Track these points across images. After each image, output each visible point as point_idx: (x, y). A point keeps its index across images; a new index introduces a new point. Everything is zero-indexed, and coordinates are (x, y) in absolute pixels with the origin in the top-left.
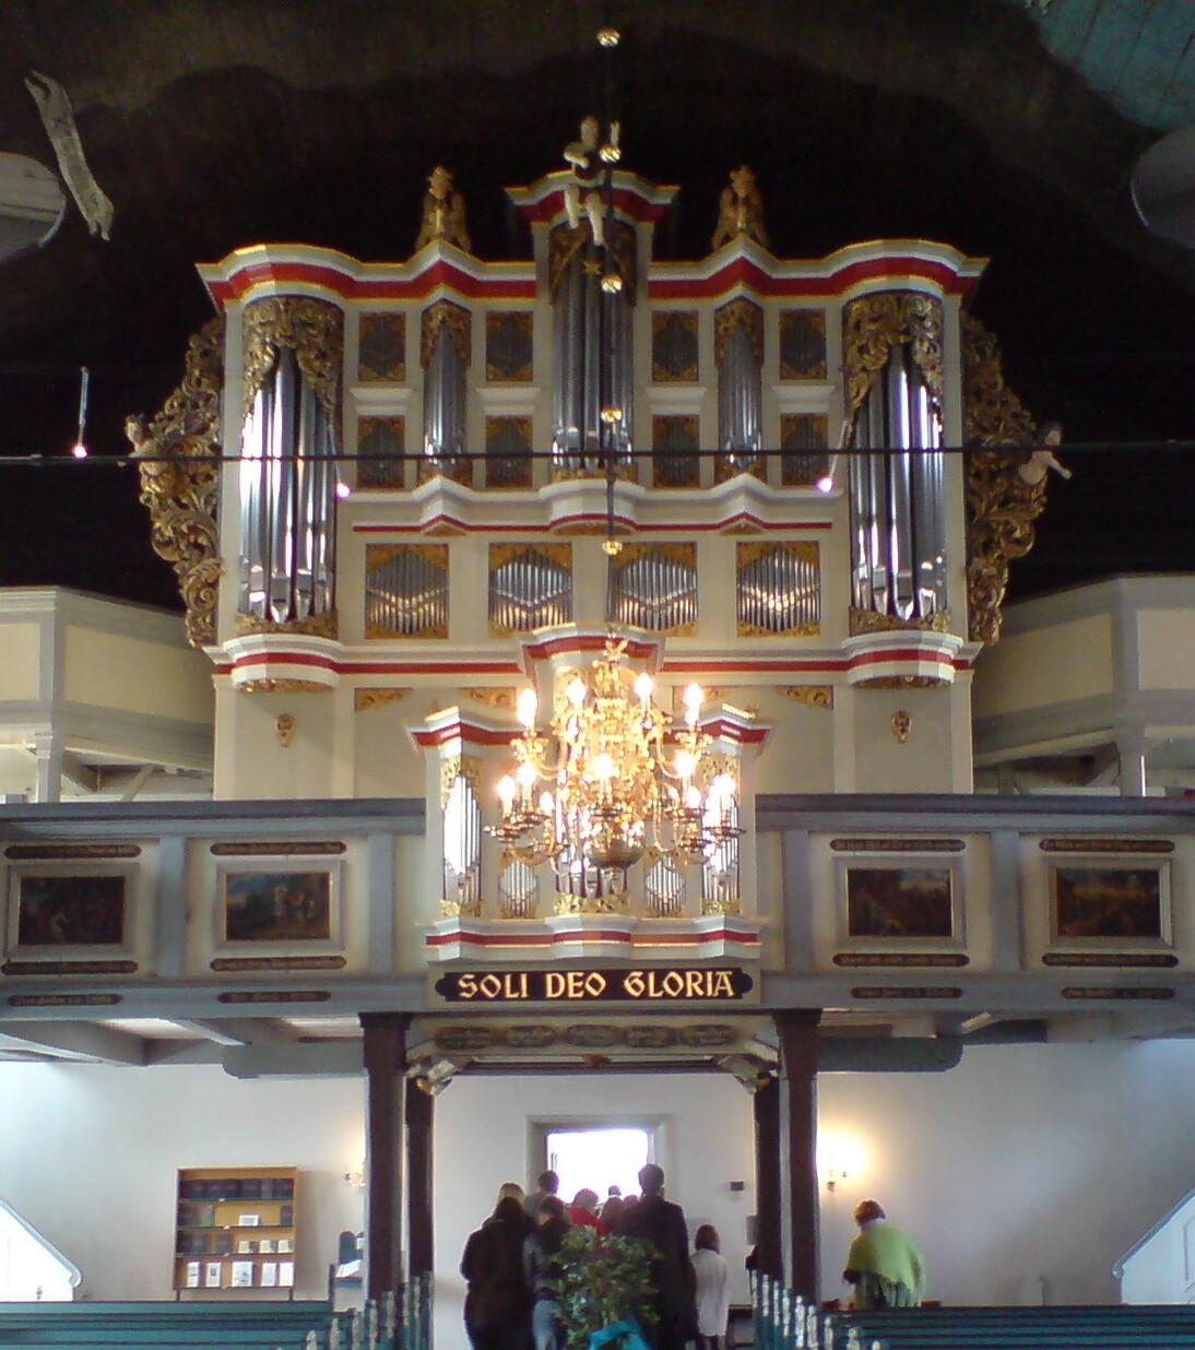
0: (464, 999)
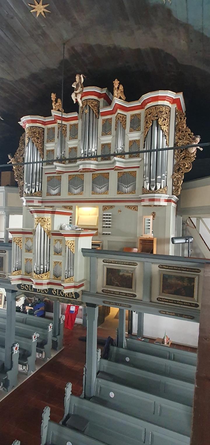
0: (22, 289)
